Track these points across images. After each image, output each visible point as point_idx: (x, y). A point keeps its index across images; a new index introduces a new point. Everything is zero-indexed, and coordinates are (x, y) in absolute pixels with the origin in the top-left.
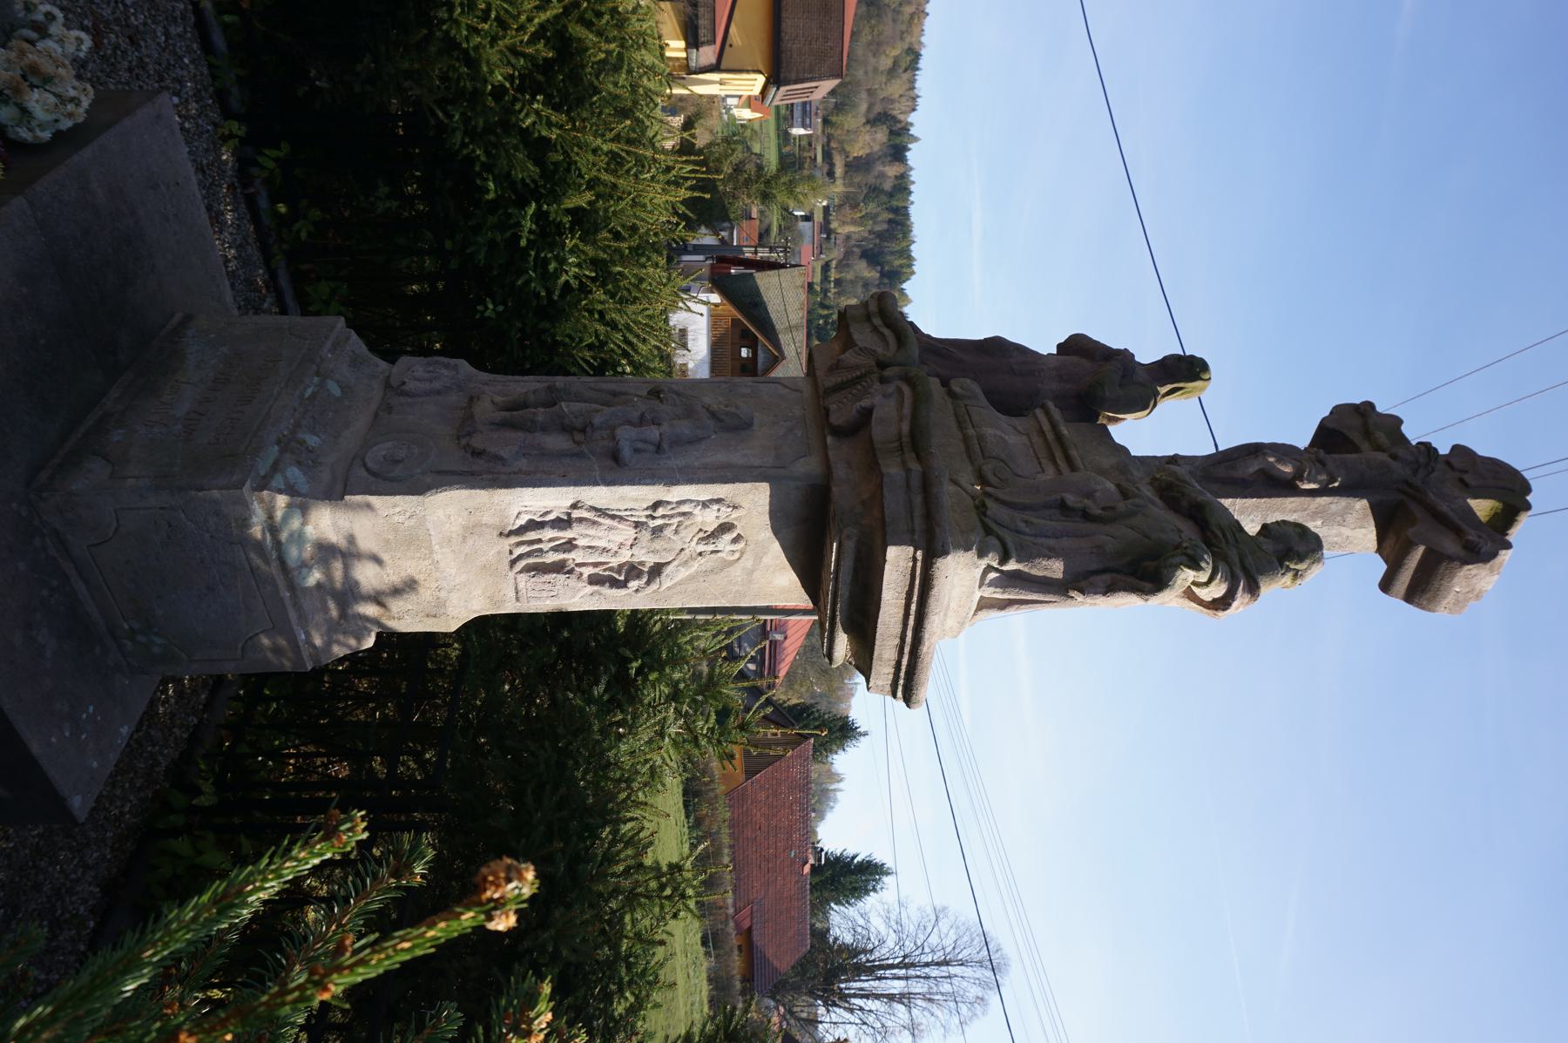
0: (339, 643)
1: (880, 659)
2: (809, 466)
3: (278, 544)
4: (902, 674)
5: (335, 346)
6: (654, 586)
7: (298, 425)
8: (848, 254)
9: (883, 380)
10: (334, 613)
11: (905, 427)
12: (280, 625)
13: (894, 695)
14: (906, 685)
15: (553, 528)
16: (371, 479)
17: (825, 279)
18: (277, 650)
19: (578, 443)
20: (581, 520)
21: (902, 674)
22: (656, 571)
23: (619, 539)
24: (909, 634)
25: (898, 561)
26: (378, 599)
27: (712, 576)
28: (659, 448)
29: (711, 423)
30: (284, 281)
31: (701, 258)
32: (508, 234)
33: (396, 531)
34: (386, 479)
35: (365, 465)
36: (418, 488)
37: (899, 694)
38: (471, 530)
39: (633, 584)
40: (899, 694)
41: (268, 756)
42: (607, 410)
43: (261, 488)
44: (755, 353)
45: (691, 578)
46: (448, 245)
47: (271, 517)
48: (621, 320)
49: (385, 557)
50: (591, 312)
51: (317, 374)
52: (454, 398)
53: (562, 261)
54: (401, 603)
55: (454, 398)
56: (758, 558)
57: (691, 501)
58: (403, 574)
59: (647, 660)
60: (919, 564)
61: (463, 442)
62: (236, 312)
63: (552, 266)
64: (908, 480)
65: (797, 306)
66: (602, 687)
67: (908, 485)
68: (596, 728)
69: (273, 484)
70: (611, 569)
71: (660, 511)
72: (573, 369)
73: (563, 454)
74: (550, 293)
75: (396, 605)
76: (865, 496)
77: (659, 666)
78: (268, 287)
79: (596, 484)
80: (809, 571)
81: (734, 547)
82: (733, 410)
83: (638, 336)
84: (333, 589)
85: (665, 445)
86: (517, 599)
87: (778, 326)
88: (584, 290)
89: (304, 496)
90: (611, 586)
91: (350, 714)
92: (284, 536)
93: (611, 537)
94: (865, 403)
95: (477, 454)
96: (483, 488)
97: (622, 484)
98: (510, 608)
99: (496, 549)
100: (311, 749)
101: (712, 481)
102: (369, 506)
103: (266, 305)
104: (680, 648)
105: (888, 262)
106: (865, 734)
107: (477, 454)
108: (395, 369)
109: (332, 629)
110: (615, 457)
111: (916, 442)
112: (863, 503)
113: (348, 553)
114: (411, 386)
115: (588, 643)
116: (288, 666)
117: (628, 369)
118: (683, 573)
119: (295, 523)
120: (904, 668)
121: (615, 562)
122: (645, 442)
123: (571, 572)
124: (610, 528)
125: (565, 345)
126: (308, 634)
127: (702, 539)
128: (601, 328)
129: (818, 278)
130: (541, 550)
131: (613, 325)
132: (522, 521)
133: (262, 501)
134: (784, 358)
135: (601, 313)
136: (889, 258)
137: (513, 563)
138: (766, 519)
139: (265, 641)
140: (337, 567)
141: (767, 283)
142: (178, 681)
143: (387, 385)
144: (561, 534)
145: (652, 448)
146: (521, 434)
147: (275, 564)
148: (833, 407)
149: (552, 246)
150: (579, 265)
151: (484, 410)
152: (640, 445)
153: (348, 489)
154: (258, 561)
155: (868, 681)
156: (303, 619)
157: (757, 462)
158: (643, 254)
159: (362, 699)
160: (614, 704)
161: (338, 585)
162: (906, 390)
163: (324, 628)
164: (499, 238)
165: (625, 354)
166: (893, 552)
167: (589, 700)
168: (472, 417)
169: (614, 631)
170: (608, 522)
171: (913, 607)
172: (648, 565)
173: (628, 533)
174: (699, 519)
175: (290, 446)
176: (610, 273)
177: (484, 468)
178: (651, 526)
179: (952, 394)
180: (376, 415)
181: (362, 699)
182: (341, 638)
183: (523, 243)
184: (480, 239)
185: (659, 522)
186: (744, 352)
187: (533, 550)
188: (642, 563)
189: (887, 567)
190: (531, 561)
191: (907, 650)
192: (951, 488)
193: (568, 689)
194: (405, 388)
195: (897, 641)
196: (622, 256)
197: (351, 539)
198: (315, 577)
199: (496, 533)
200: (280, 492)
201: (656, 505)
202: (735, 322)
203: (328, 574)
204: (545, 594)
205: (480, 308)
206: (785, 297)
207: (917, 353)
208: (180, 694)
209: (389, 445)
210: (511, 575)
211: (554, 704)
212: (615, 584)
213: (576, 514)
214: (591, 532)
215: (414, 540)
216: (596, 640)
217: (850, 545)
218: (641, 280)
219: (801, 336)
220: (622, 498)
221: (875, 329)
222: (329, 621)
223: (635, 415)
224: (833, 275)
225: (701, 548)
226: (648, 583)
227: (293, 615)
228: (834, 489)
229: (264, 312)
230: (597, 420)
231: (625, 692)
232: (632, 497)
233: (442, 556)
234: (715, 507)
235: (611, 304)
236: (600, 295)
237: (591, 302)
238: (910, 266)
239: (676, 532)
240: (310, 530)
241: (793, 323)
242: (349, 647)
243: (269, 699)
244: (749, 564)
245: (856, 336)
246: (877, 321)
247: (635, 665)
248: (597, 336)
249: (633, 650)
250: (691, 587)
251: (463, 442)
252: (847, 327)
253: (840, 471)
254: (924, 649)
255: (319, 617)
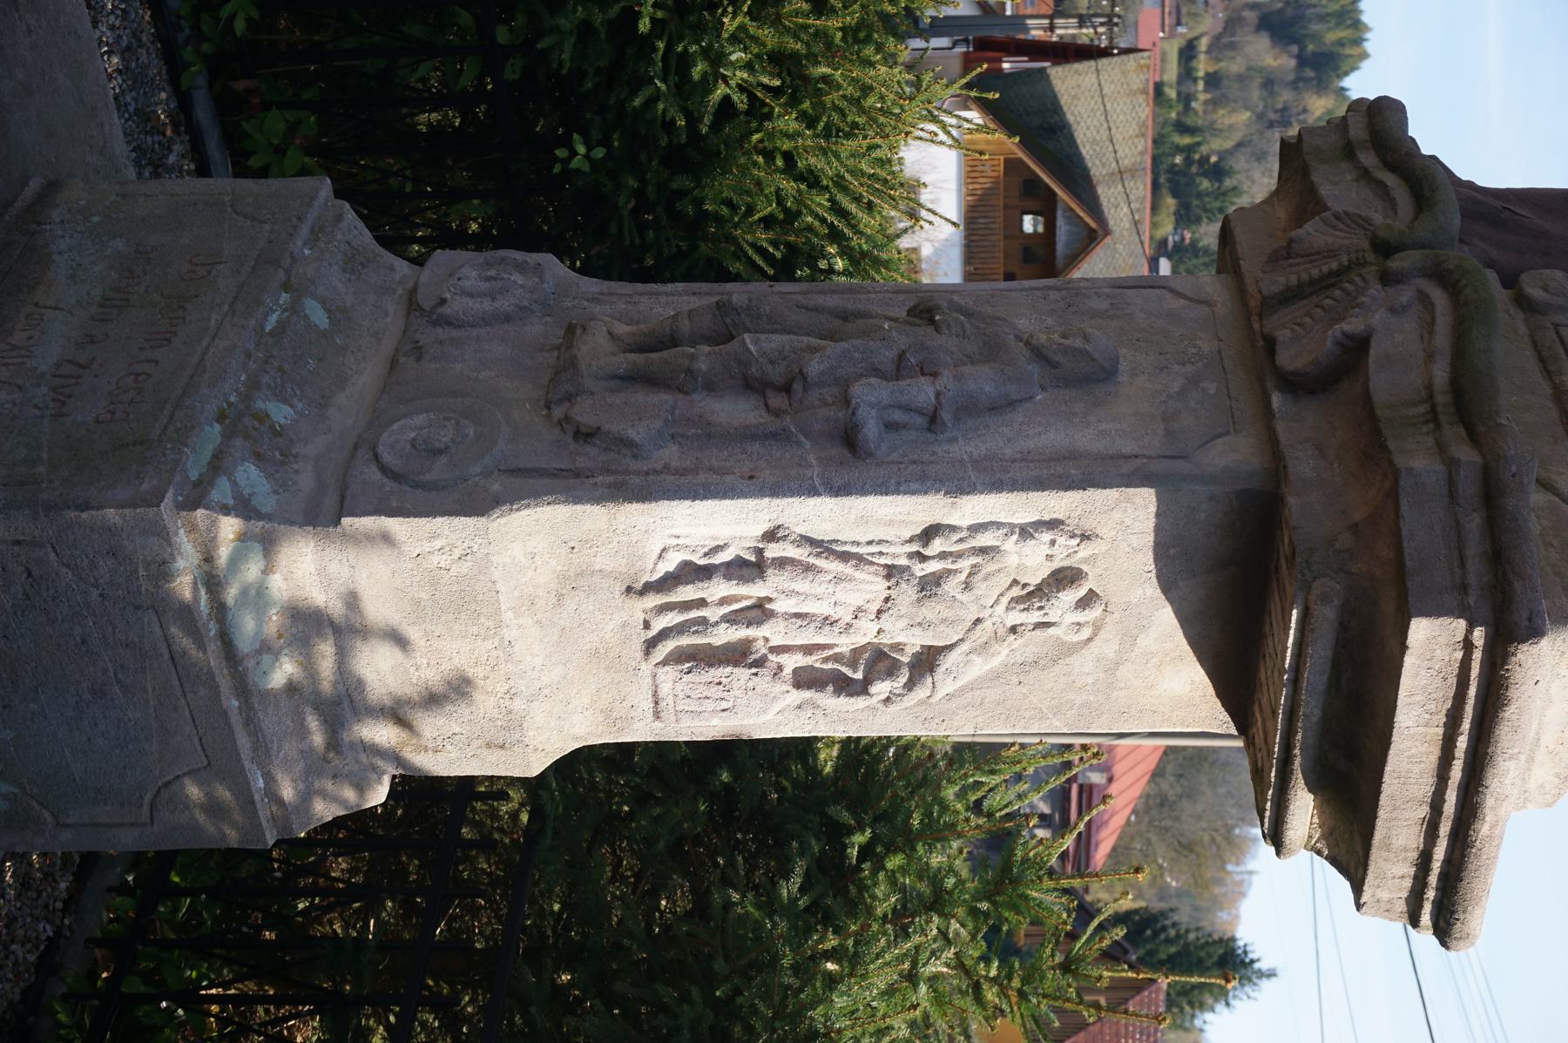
0: (324, 795)
1: (1387, 847)
2: (1234, 455)
3: (220, 609)
4: (1433, 879)
5: (315, 235)
6: (921, 692)
7: (254, 385)
8: (1232, 24)
9: (1387, 278)
10: (318, 739)
11: (1441, 374)
12: (220, 763)
13: (1414, 921)
14: (1441, 901)
15: (728, 577)
16: (389, 485)
17: (1187, 74)
18: (214, 809)
19: (777, 413)
20: (782, 563)
21: (1433, 879)
22: (926, 662)
23: (856, 600)
24: (1451, 797)
25: (1432, 649)
26: (397, 713)
27: (1035, 673)
28: (933, 420)
29: (1034, 369)
30: (203, 113)
31: (944, 42)
32: (614, 11)
33: (434, 584)
34: (417, 486)
35: (376, 458)
36: (475, 502)
37: (1426, 918)
38: (573, 582)
39: (881, 688)
40: (1426, 918)
41: (178, 999)
42: (834, 349)
43: (192, 504)
44: (1050, 226)
45: (995, 677)
46: (502, 35)
47: (209, 559)
48: (827, 168)
49: (413, 633)
50: (769, 156)
51: (286, 287)
52: (535, 328)
53: (717, 59)
54: (441, 721)
55: (535, 328)
56: (1129, 639)
57: (998, 525)
58: (446, 666)
59: (883, 830)
60: (1477, 655)
61: (558, 412)
62: (131, 173)
63: (698, 70)
64: (1451, 482)
65: (1133, 129)
66: (796, 881)
67: (1452, 495)
68: (786, 962)
69: (215, 496)
70: (837, 658)
71: (937, 545)
72: (736, 267)
73: (747, 435)
74: (693, 121)
75: (431, 725)
76: (1357, 516)
77: (905, 840)
78: (175, 125)
79: (813, 492)
80: (1234, 667)
81: (1081, 617)
82: (1078, 343)
83: (857, 199)
84: (316, 693)
85: (946, 415)
86: (657, 715)
87: (1097, 171)
88: (758, 112)
89: (269, 517)
90: (838, 691)
91: (318, 920)
92: (231, 594)
93: (840, 596)
94: (1353, 325)
95: (585, 435)
96: (597, 500)
97: (863, 492)
98: (642, 731)
99: (618, 618)
100: (251, 987)
101: (1040, 485)
102: (386, 538)
103: (172, 159)
104: (944, 807)
105: (1314, 37)
106: (1271, 974)
107: (585, 435)
108: (426, 275)
109: (315, 769)
110: (850, 440)
111: (1465, 404)
112: (1354, 528)
113: (343, 627)
114: (457, 306)
115: (764, 795)
116: (233, 838)
117: (840, 264)
118: (979, 667)
119: (252, 570)
120: (1436, 866)
121: (845, 644)
122: (907, 408)
123: (760, 663)
124: (838, 579)
125: (718, 219)
126: (269, 778)
127: (1016, 600)
128: (789, 186)
129: (1172, 73)
130: (704, 621)
131: (812, 180)
132: (670, 564)
133: (193, 529)
134: (1107, 232)
135: (789, 157)
136: (1315, 27)
137: (651, 645)
138: (1147, 560)
139: (194, 791)
140: (326, 653)
141: (1073, 86)
142: (21, 858)
143: (412, 304)
144: (743, 590)
145: (919, 421)
146: (665, 398)
147: (213, 647)
148: (1283, 335)
149: (698, 30)
150: (749, 66)
151: (597, 350)
152: (897, 416)
153: (345, 508)
154: (184, 642)
155: (1358, 889)
156: (262, 750)
157: (1127, 447)
158: (868, 40)
159: (337, 897)
160: (819, 916)
161: (326, 686)
162: (1439, 296)
163: (299, 767)
164: (598, 19)
165: (835, 235)
166: (1420, 631)
167: (770, 905)
168: (573, 363)
169: (814, 770)
170: (834, 566)
171: (1462, 743)
172: (910, 651)
173: (871, 587)
174: (1012, 560)
175: (239, 422)
176: (806, 79)
177: (595, 462)
178: (918, 573)
179: (1523, 302)
180: (393, 363)
181: (337, 897)
182: (329, 785)
183: (644, 25)
184: (564, 23)
185: (933, 566)
186: (1029, 224)
187: (689, 619)
188: (899, 647)
189: (1409, 660)
190: (685, 641)
191: (1445, 828)
192: (1537, 497)
193: (727, 882)
194: (445, 310)
195: (1424, 811)
196: (829, 44)
197: (352, 600)
198: (284, 671)
199: (619, 588)
200: (226, 510)
201: (929, 533)
202: (1012, 165)
203: (309, 665)
204: (709, 706)
205: (561, 153)
206: (1107, 113)
207: (1457, 220)
208: (24, 881)
209: (420, 419)
210: (647, 668)
211: (700, 910)
212: (845, 686)
213: (773, 551)
214: (802, 585)
215: (467, 602)
216: (780, 789)
217: (1326, 615)
218: (866, 90)
219: (1141, 189)
220: (863, 520)
221: (1365, 174)
222: (307, 753)
223: (887, 356)
224: (1202, 66)
225: (1015, 617)
226: (910, 685)
227: (243, 742)
228: (1292, 501)
229: (170, 170)
230: (814, 367)
231: (837, 891)
232: (883, 518)
233: (513, 631)
234: (1046, 537)
235: (808, 139)
236: (789, 122)
237: (771, 135)
238: (1358, 42)
239: (967, 586)
240: (279, 586)
241: (1125, 163)
242: (343, 803)
243: (177, 892)
244: (1110, 651)
245: (1325, 190)
246: (1368, 159)
247: (859, 839)
248: (780, 202)
249: (851, 808)
250: (992, 694)
251: (558, 412)
252: (1305, 172)
253: (1302, 465)
254: (1484, 829)
255: (290, 748)
